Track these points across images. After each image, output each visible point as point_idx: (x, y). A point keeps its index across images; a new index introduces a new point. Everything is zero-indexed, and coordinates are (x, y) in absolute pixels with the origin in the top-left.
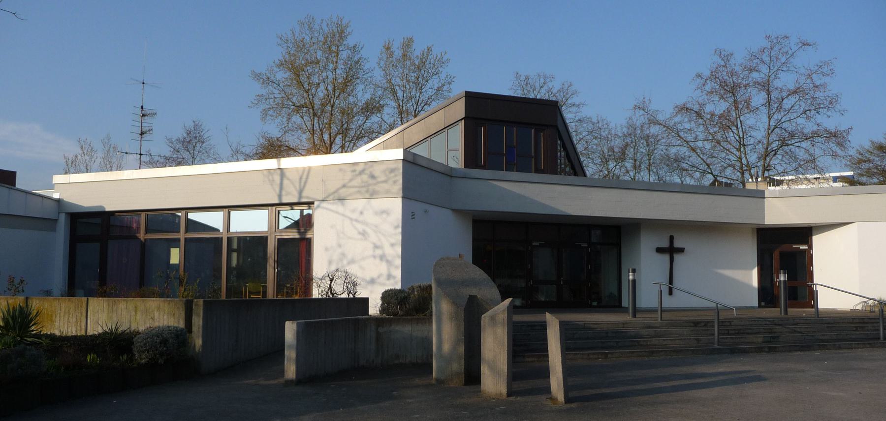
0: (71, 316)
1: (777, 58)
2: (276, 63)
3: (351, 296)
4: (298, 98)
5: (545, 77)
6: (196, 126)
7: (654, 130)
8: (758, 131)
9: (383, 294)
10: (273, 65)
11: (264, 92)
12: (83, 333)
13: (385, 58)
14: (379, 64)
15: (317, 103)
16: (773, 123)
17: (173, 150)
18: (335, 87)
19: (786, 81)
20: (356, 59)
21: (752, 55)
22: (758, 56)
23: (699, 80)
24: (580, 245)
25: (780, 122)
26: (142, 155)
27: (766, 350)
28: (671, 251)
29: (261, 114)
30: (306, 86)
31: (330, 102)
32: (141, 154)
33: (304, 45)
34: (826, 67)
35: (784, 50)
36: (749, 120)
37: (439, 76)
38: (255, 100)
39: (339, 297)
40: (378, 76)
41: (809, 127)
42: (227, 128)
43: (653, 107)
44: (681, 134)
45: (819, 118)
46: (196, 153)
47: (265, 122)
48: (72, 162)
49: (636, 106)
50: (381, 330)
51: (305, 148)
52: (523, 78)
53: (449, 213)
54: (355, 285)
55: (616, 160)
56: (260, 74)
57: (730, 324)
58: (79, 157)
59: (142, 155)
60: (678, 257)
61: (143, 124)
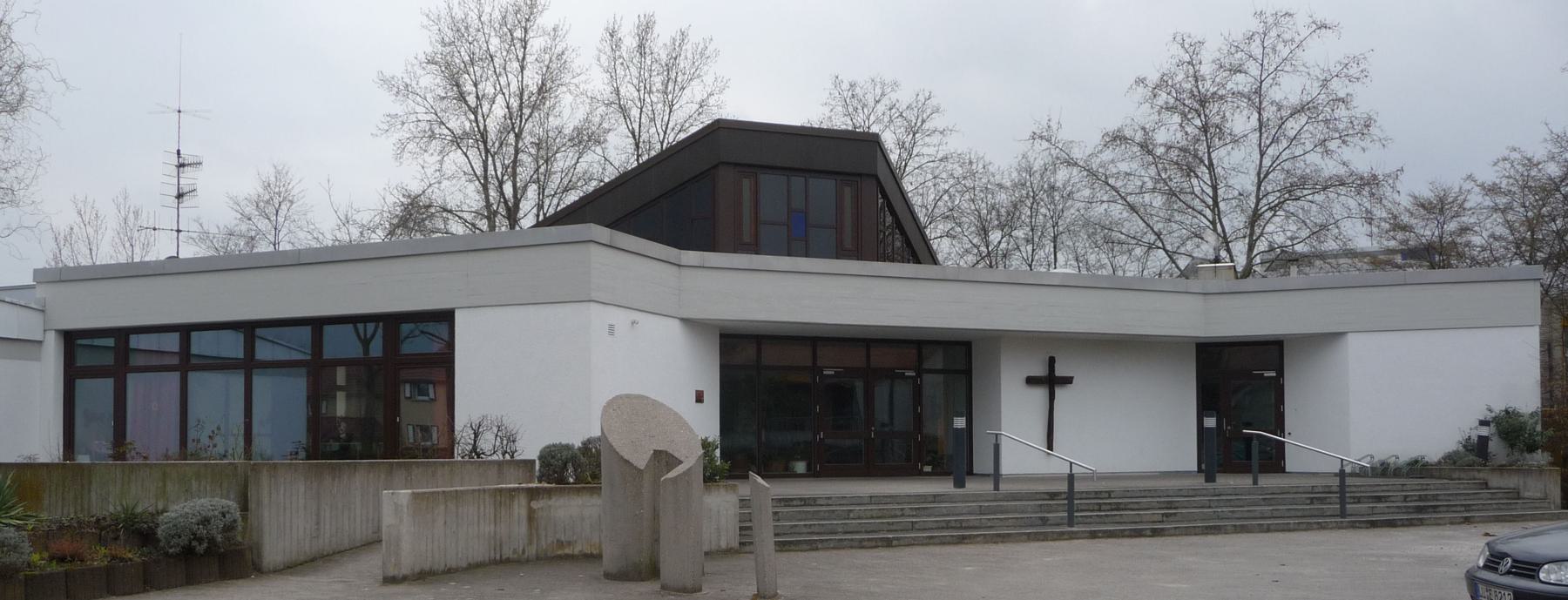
0: (67, 489)
1: (1274, 50)
2: (419, 58)
3: (508, 457)
4: (459, 122)
5: (883, 84)
6: (278, 172)
7: (1062, 175)
8: (1243, 175)
9: (541, 452)
10: (415, 62)
11: (398, 108)
12: (130, 260)
13: (608, 49)
14: (599, 60)
15: (493, 126)
16: (1267, 162)
17: (240, 216)
18: (522, 103)
19: (1288, 89)
20: (559, 49)
21: (1231, 45)
22: (1242, 46)
23: (1140, 89)
24: (904, 373)
25: (1278, 162)
26: (181, 231)
27: (1148, 533)
28: (1051, 381)
29: (395, 148)
30: (472, 100)
31: (513, 129)
32: (178, 231)
33: (467, 28)
34: (1355, 65)
35: (1287, 36)
36: (1225, 157)
37: (702, 81)
38: (383, 122)
39: (490, 458)
40: (598, 83)
41: (1330, 168)
42: (329, 181)
43: (1063, 135)
44: (1111, 181)
45: (1347, 153)
46: (281, 220)
47: (401, 163)
48: (66, 240)
49: (1034, 133)
50: (534, 505)
51: (473, 210)
52: (845, 86)
53: (675, 325)
54: (512, 439)
55: (1001, 227)
56: (393, 78)
57: (1110, 495)
58: (76, 229)
59: (181, 231)
60: (1060, 393)
61: (181, 180)
